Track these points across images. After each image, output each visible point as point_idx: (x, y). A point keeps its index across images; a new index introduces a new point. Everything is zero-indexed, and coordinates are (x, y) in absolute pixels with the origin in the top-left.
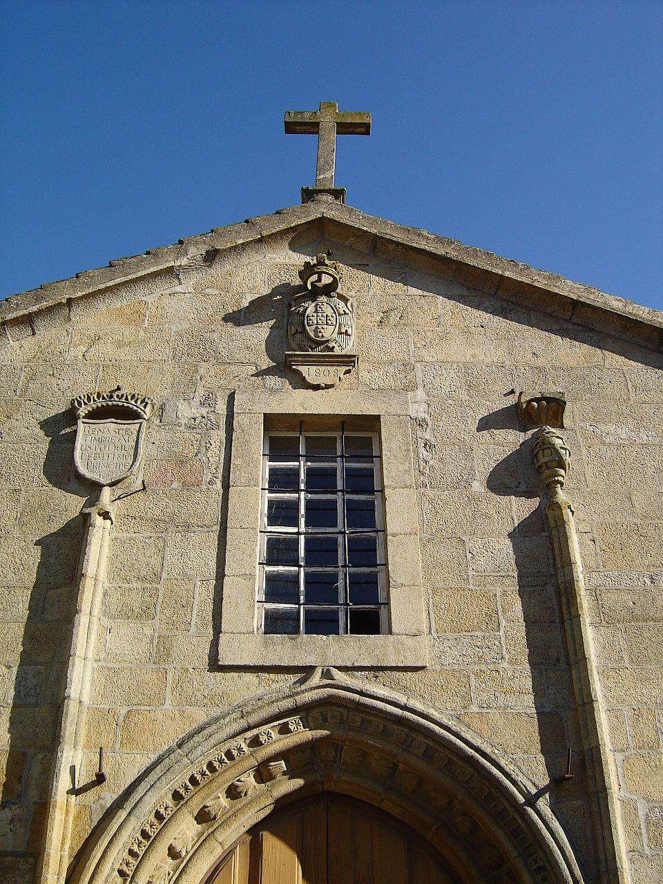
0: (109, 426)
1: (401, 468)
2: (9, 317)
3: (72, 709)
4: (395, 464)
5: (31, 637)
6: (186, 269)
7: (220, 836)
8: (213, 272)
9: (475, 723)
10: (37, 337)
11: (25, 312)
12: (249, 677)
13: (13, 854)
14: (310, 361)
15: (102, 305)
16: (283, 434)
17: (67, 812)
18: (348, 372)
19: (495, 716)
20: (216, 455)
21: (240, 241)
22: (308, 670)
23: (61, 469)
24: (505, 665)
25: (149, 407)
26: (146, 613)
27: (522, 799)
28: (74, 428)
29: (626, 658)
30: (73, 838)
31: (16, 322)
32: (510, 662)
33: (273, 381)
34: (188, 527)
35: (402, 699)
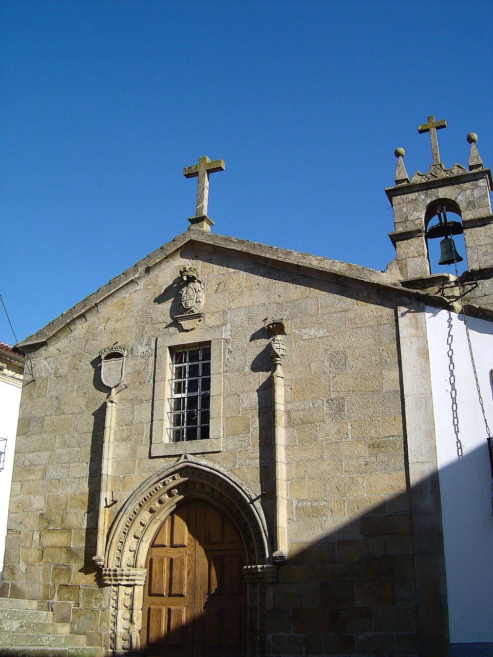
0: (113, 361)
1: (218, 365)
2: (75, 317)
3: (104, 478)
4: (216, 364)
5: (92, 452)
6: (139, 278)
7: (157, 518)
8: (150, 276)
9: (237, 472)
10: (88, 322)
11: (80, 313)
12: (162, 460)
13: (92, 528)
14: (183, 319)
15: (109, 302)
16: (177, 352)
17: (105, 514)
18: (199, 321)
19: (245, 469)
20: (150, 368)
21: (158, 261)
22: (180, 456)
23: (99, 384)
24: (250, 447)
25: (126, 351)
26: (128, 438)
27: (248, 501)
28: (100, 364)
29: (297, 441)
30: (108, 522)
31: (78, 318)
32: (252, 446)
33: (172, 329)
34: (141, 402)
35: (211, 465)
